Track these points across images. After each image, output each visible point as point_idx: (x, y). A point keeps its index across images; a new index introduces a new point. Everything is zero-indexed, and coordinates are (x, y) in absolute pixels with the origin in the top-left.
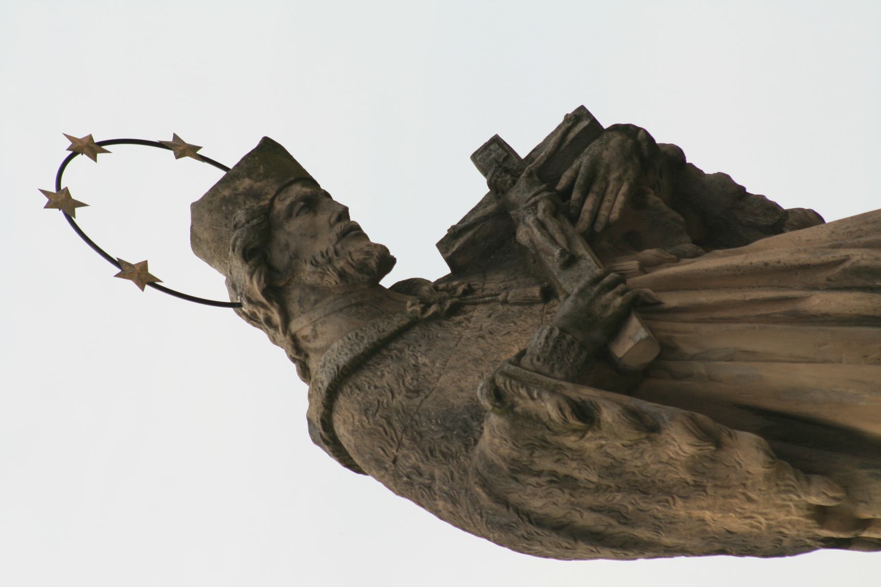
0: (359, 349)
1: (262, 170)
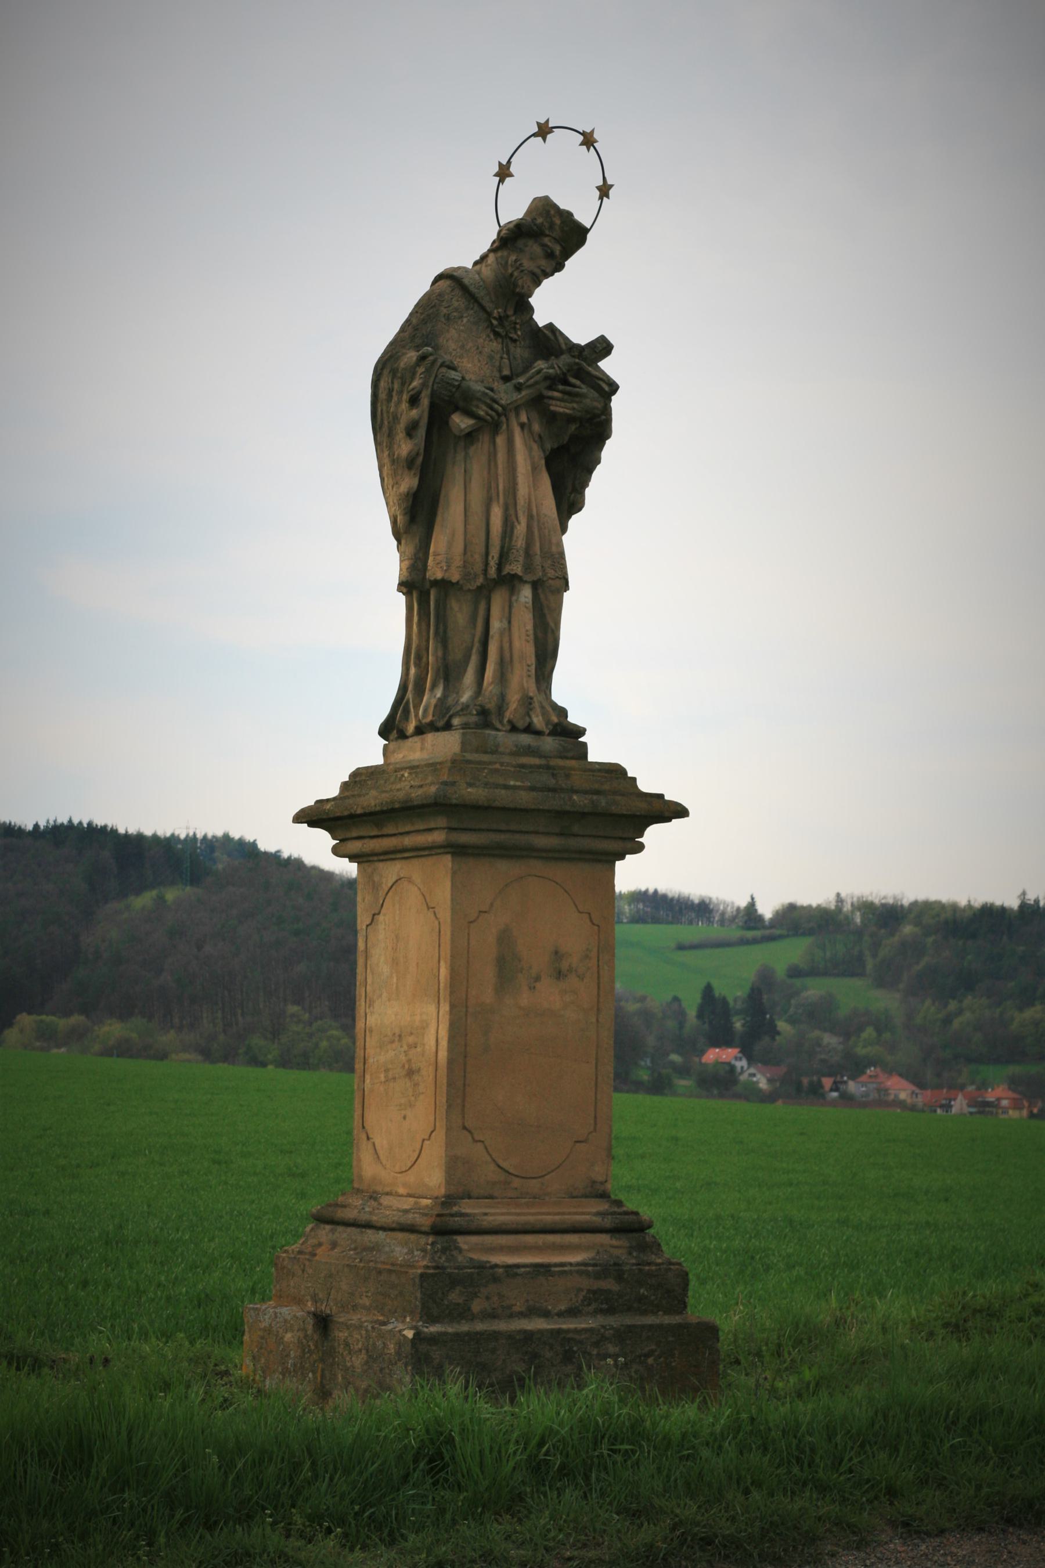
0: (472, 288)
1: (566, 229)
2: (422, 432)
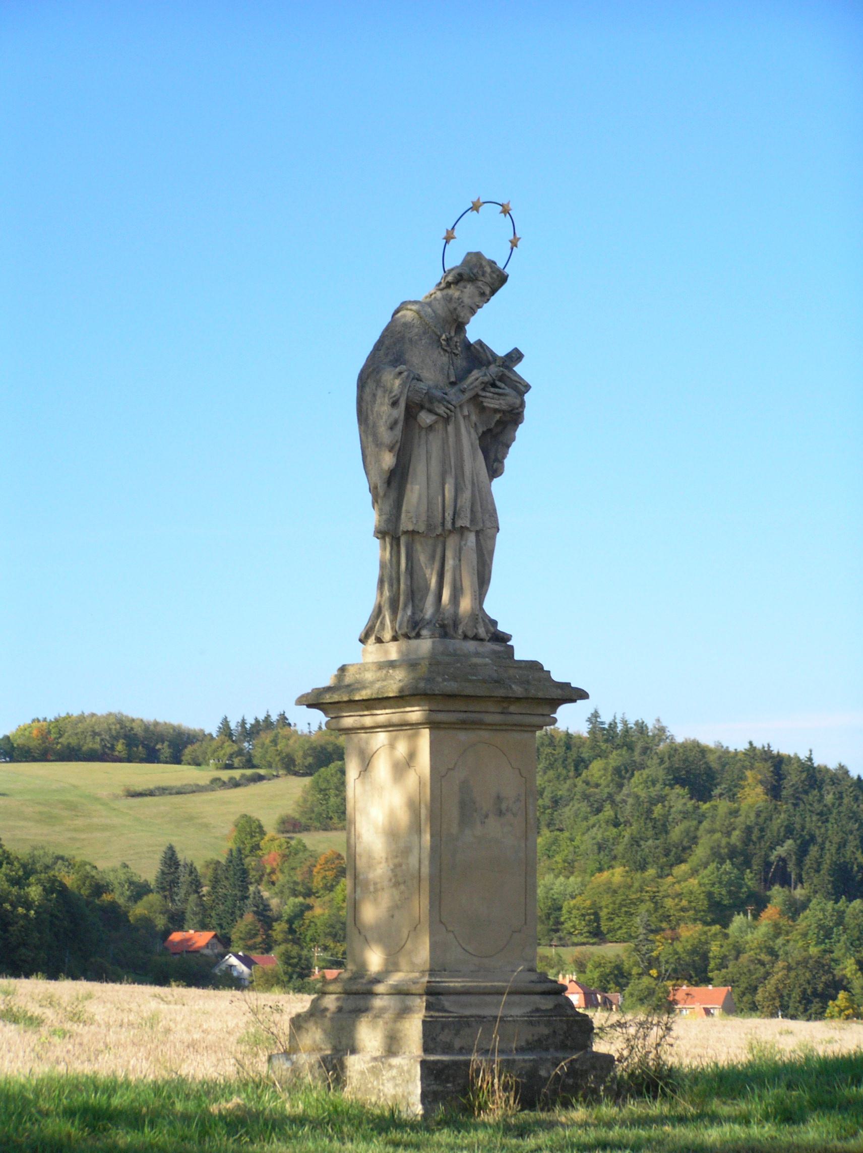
2: (400, 426)
